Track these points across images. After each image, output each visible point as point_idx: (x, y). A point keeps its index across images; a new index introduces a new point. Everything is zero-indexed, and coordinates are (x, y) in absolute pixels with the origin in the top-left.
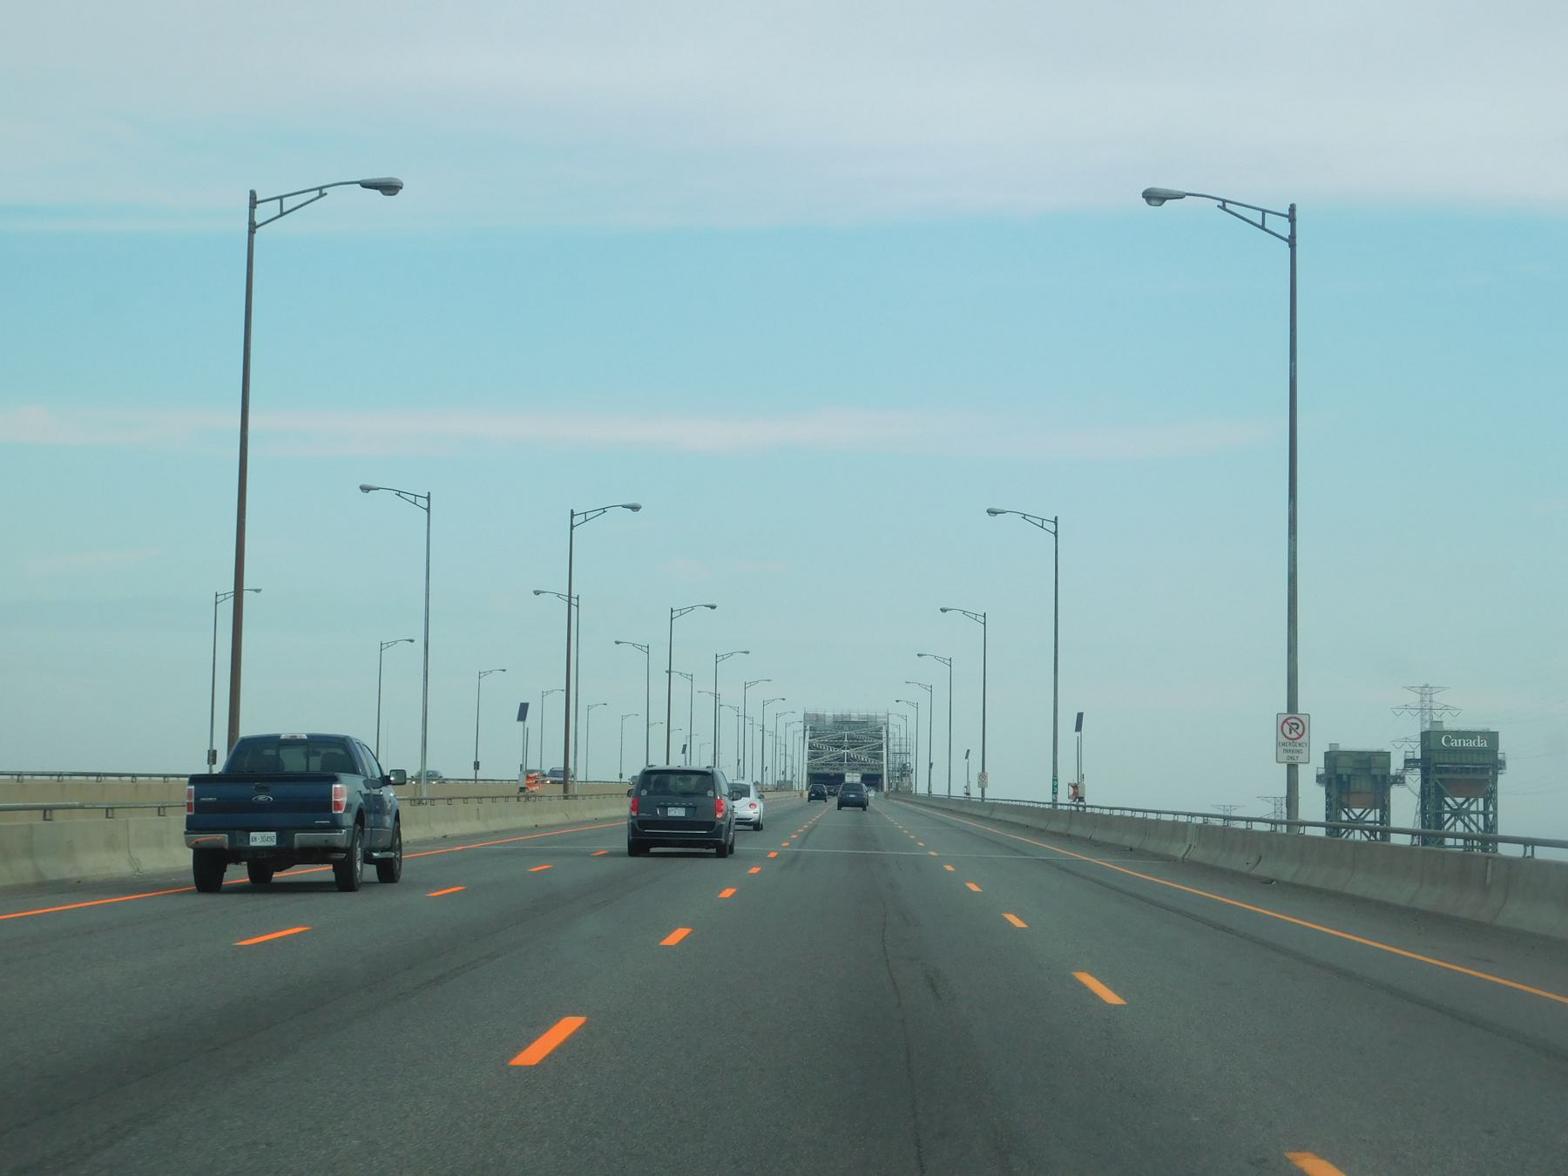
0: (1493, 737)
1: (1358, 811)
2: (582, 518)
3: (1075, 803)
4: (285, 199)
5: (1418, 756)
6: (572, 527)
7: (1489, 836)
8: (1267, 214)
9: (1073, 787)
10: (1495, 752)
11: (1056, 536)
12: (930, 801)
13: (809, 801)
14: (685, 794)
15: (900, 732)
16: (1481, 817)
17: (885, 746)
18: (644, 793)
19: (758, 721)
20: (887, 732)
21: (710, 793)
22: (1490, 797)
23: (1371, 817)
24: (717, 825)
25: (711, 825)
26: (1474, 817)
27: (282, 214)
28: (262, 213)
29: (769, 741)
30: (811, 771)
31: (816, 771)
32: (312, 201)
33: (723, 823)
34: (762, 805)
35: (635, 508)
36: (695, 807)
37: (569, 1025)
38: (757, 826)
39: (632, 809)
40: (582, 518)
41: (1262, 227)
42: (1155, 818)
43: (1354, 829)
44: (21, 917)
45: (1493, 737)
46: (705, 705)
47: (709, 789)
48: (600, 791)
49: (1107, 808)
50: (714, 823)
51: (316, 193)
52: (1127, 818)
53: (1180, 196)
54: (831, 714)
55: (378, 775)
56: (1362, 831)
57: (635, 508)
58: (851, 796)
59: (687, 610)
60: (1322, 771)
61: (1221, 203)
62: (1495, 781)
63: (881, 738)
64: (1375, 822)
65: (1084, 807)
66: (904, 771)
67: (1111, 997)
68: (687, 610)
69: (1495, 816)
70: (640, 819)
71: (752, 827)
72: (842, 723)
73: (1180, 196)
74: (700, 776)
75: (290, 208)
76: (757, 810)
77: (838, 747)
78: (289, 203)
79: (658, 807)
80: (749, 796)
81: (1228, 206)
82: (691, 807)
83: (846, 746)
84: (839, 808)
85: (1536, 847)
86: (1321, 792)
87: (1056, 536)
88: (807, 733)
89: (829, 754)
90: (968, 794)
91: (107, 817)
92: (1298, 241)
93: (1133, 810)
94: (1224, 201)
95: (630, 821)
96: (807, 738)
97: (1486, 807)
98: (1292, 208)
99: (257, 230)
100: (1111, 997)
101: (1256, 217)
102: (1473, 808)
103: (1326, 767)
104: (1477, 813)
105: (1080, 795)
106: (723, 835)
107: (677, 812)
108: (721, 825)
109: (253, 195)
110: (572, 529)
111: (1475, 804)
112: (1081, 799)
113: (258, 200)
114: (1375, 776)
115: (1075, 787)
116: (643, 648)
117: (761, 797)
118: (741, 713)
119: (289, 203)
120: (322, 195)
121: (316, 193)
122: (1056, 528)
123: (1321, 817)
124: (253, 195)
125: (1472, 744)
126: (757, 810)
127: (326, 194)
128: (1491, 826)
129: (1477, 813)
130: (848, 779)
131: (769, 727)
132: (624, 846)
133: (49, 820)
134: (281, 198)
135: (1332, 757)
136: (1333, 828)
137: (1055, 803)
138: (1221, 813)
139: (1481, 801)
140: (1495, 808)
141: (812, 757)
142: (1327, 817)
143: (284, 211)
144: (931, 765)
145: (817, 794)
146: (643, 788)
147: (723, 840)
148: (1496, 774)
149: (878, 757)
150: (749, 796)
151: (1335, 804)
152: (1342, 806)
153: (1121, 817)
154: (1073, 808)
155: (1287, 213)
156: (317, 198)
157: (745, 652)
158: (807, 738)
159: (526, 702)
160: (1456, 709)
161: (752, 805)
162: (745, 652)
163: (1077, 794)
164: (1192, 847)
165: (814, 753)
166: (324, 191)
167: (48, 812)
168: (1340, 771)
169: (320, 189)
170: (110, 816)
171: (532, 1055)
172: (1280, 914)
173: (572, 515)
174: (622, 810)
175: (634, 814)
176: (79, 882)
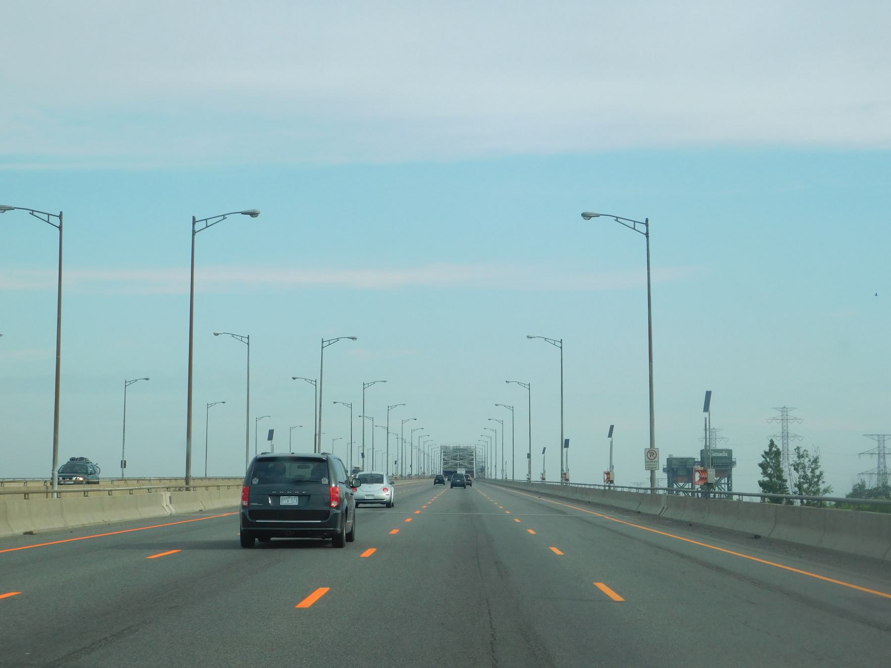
0: (730, 452)
1: (681, 484)
2: (327, 343)
3: (608, 484)
4: (208, 220)
5: (699, 460)
6: (194, 233)
7: (730, 495)
8: (636, 223)
9: (607, 474)
10: (731, 458)
11: (561, 349)
12: (496, 482)
13: (435, 484)
14: (299, 482)
15: (480, 453)
16: (726, 485)
17: (474, 459)
18: (255, 481)
19: (422, 450)
20: (476, 453)
21: (325, 481)
22: (729, 477)
23: (687, 487)
24: (331, 514)
25: (324, 515)
26: (723, 486)
27: (207, 227)
28: (198, 227)
29: (414, 451)
30: (444, 470)
31: (446, 470)
32: (220, 221)
33: (339, 512)
34: (393, 489)
35: (253, 214)
36: (309, 496)
37: (321, 591)
38: (389, 505)
39: (244, 498)
40: (391, 408)
41: (634, 229)
42: (627, 491)
43: (680, 491)
44: (20, 547)
45: (730, 452)
46: (381, 434)
47: (324, 476)
48: (213, 483)
49: (597, 485)
50: (329, 512)
51: (222, 217)
52: (587, 488)
53: (598, 216)
54: (452, 446)
55: (400, 473)
56: (683, 492)
57: (253, 214)
58: (458, 481)
59: (335, 341)
60: (665, 467)
61: (616, 219)
62: (731, 470)
63: (473, 456)
64: (689, 489)
65: (615, 487)
66: (483, 469)
67: (616, 597)
68: (335, 341)
69: (731, 485)
70: (251, 509)
71: (385, 505)
72: (457, 449)
73: (598, 216)
74: (316, 464)
75: (210, 224)
76: (389, 492)
77: (455, 460)
78: (210, 222)
79: (270, 495)
80: (382, 483)
81: (619, 220)
82: (304, 495)
83: (458, 459)
84: (452, 487)
85: (743, 496)
86: (665, 476)
87: (561, 349)
88: (442, 454)
89: (452, 462)
90: (544, 479)
91: (25, 499)
92: (649, 235)
93: (622, 487)
94: (617, 217)
95: (242, 511)
96: (442, 456)
97: (728, 481)
98: (647, 220)
99: (196, 234)
100: (616, 597)
101: (553, 342)
102: (723, 481)
103: (668, 465)
104: (724, 484)
105: (611, 479)
106: (339, 526)
107: (289, 501)
108: (337, 514)
109: (194, 218)
110: (193, 234)
111: (724, 479)
112: (612, 482)
113: (196, 220)
114: (688, 469)
115: (608, 474)
116: (638, 226)
117: (392, 483)
118: (357, 411)
119: (210, 222)
120: (224, 218)
121: (222, 217)
122: (562, 345)
123: (666, 486)
124: (194, 218)
125: (721, 455)
126: (389, 492)
127: (226, 218)
128: (730, 489)
129: (724, 484)
130: (459, 472)
131: (415, 443)
132: (235, 534)
133: (27, 499)
134: (206, 220)
135: (670, 461)
136: (670, 489)
137: (653, 489)
138: (636, 486)
139: (726, 478)
140: (731, 482)
141: (444, 464)
142: (668, 486)
143: (208, 225)
144: (529, 456)
145: (439, 480)
146: (254, 476)
147: (339, 529)
148: (731, 467)
149: (472, 464)
150: (382, 483)
151: (671, 482)
152: (676, 482)
153: (622, 492)
154: (607, 488)
155: (645, 222)
156: (222, 220)
157: (384, 381)
158: (442, 456)
159: (272, 429)
160: (726, 438)
161: (385, 489)
162: (384, 381)
163: (609, 478)
164: (665, 508)
165: (446, 462)
166: (225, 216)
167: (86, 493)
168: (673, 467)
169: (224, 215)
170: (26, 498)
171: (307, 603)
172: (804, 574)
173: (323, 342)
174: (234, 500)
175: (245, 503)
176: (109, 524)
